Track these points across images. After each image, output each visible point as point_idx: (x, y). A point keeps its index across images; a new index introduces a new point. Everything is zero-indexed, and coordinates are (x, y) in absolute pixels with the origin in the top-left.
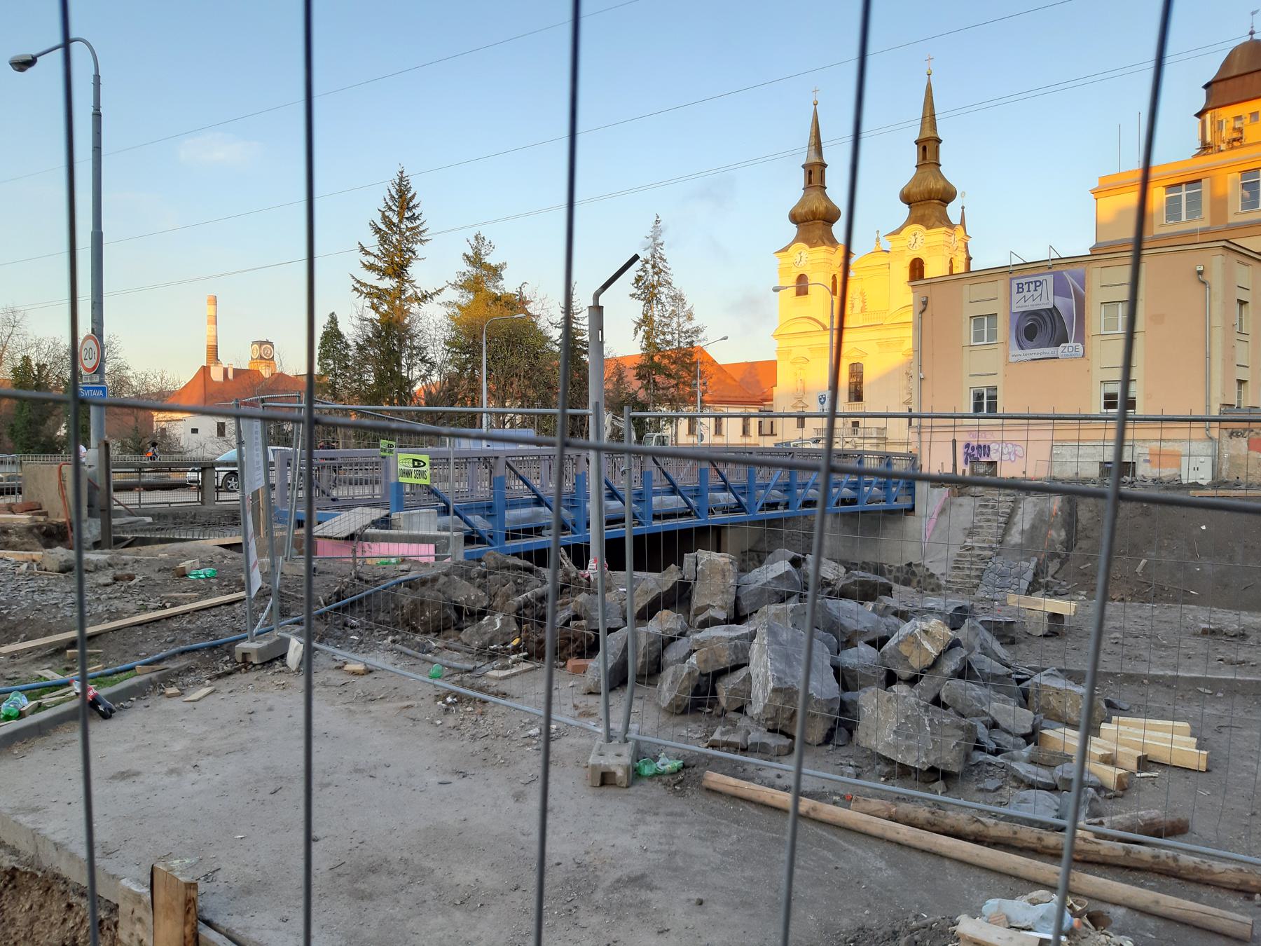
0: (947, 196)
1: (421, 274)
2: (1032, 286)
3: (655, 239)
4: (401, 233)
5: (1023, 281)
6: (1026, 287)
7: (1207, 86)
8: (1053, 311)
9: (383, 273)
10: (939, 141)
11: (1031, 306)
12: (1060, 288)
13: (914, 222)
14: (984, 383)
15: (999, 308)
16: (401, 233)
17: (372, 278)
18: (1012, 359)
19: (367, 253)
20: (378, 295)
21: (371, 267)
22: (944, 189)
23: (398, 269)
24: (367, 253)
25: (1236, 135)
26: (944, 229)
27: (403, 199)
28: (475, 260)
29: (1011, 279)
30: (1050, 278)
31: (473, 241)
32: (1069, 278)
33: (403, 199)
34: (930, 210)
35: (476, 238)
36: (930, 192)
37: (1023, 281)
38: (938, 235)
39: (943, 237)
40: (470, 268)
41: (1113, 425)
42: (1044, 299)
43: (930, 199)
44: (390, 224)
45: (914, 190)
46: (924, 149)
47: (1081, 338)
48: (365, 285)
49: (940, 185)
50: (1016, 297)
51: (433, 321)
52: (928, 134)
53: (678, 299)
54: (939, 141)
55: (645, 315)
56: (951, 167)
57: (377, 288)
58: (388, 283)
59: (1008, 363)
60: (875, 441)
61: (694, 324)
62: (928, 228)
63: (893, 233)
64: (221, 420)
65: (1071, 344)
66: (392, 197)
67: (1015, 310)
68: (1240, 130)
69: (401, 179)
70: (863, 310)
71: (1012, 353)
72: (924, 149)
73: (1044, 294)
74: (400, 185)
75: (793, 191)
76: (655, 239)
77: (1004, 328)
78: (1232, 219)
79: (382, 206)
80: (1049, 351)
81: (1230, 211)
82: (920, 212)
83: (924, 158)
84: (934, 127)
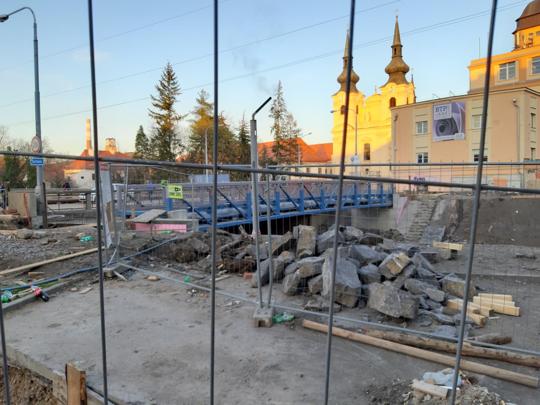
0: (405, 70)
1: (178, 108)
2: (443, 109)
3: (279, 91)
4: (169, 90)
5: (439, 106)
6: (440, 109)
7: (517, 21)
8: (452, 120)
9: (163, 108)
10: (402, 46)
11: (442, 117)
12: (455, 109)
13: (391, 82)
14: (422, 151)
15: (428, 118)
17: (157, 110)
18: (434, 141)
19: (155, 99)
20: (160, 117)
22: (404, 67)
23: (168, 106)
24: (155, 99)
25: (530, 42)
26: (404, 84)
29: (433, 106)
30: (450, 105)
31: (200, 93)
32: (459, 106)
33: (170, 76)
36: (398, 68)
37: (439, 106)
40: (199, 105)
42: (448, 114)
43: (398, 71)
44: (164, 86)
45: (391, 68)
46: (395, 50)
47: (464, 131)
49: (402, 65)
50: (435, 113)
52: (397, 43)
53: (290, 117)
54: (402, 46)
55: (276, 125)
56: (407, 58)
58: (164, 112)
59: (432, 142)
62: (397, 84)
63: (382, 87)
65: (460, 133)
66: (165, 75)
67: (435, 119)
68: (532, 40)
69: (168, 66)
70: (370, 120)
71: (434, 138)
72: (395, 50)
73: (448, 112)
75: (339, 69)
76: (279, 91)
77: (431, 127)
78: (528, 78)
80: (450, 137)
81: (528, 75)
82: (394, 78)
83: (395, 54)
84: (399, 40)
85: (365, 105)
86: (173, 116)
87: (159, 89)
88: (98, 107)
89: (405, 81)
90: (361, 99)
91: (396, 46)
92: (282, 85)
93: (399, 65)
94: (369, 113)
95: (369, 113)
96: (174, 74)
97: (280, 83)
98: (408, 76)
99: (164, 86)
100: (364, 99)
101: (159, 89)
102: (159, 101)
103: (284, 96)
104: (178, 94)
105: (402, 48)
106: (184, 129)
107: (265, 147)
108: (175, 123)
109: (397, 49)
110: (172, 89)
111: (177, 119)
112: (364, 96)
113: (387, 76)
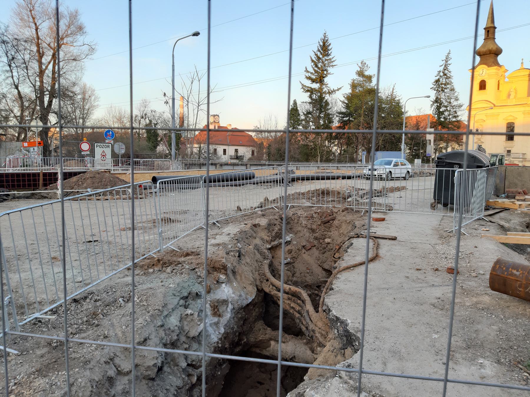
0: (498, 52)
1: (330, 82)
3: (446, 62)
4: (323, 62)
9: (313, 81)
10: (495, 28)
16: (323, 62)
17: (308, 83)
19: (308, 72)
20: (311, 91)
21: (309, 78)
22: (497, 48)
23: (320, 79)
24: (308, 72)
26: (496, 67)
27: (325, 48)
28: (360, 73)
31: (360, 65)
33: (325, 48)
34: (491, 59)
35: (362, 63)
38: (493, 70)
39: (494, 71)
40: (358, 77)
41: (60, 203)
43: (490, 54)
44: (319, 58)
46: (488, 31)
48: (305, 86)
49: (494, 48)
51: (337, 102)
52: (490, 25)
53: (453, 90)
54: (495, 28)
55: (437, 98)
56: (500, 40)
57: (311, 88)
58: (316, 86)
60: (521, 160)
61: (459, 102)
64: (236, 147)
66: (320, 45)
69: (325, 37)
70: (515, 97)
72: (488, 31)
74: (324, 40)
76: (446, 62)
79: (316, 50)
83: (488, 36)
84: (493, 21)
85: (507, 80)
86: (325, 89)
87: (313, 61)
88: (129, 103)
89: (497, 64)
90: (503, 73)
91: (491, 27)
92: (450, 56)
93: (491, 46)
94: (516, 90)
95: (516, 90)
96: (330, 44)
97: (449, 53)
98: (500, 58)
99: (319, 58)
100: (507, 74)
101: (313, 61)
102: (312, 73)
103: (450, 68)
104: (332, 66)
105: (496, 30)
106: (337, 102)
107: (418, 122)
108: (327, 97)
109: (490, 31)
110: (326, 60)
111: (329, 93)
112: (506, 71)
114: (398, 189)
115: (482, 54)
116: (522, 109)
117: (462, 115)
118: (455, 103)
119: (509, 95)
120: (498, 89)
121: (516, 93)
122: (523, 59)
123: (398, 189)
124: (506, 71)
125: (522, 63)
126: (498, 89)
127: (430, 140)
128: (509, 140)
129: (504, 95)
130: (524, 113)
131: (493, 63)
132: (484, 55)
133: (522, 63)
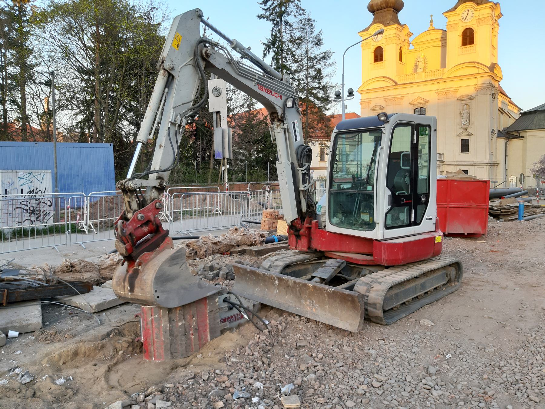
38: (391, 31)
39: (394, 31)
43: (387, 7)
55: (274, 37)
62: (478, 4)
70: (424, 70)
85: (411, 47)
90: (406, 38)
94: (425, 59)
98: (401, 16)
106: (46, 110)
112: (410, 35)
113: (371, 16)
114: (534, 218)
115: (375, 8)
116: (435, 87)
117: (330, 75)
118: (317, 51)
119: (416, 68)
120: (401, 60)
121: (425, 63)
122: (432, 16)
123: (534, 218)
124: (410, 35)
125: (431, 22)
126: (401, 60)
127: (218, 113)
128: (468, 151)
129: (409, 67)
130: (438, 93)
131: (392, 20)
132: (378, 10)
133: (431, 22)
